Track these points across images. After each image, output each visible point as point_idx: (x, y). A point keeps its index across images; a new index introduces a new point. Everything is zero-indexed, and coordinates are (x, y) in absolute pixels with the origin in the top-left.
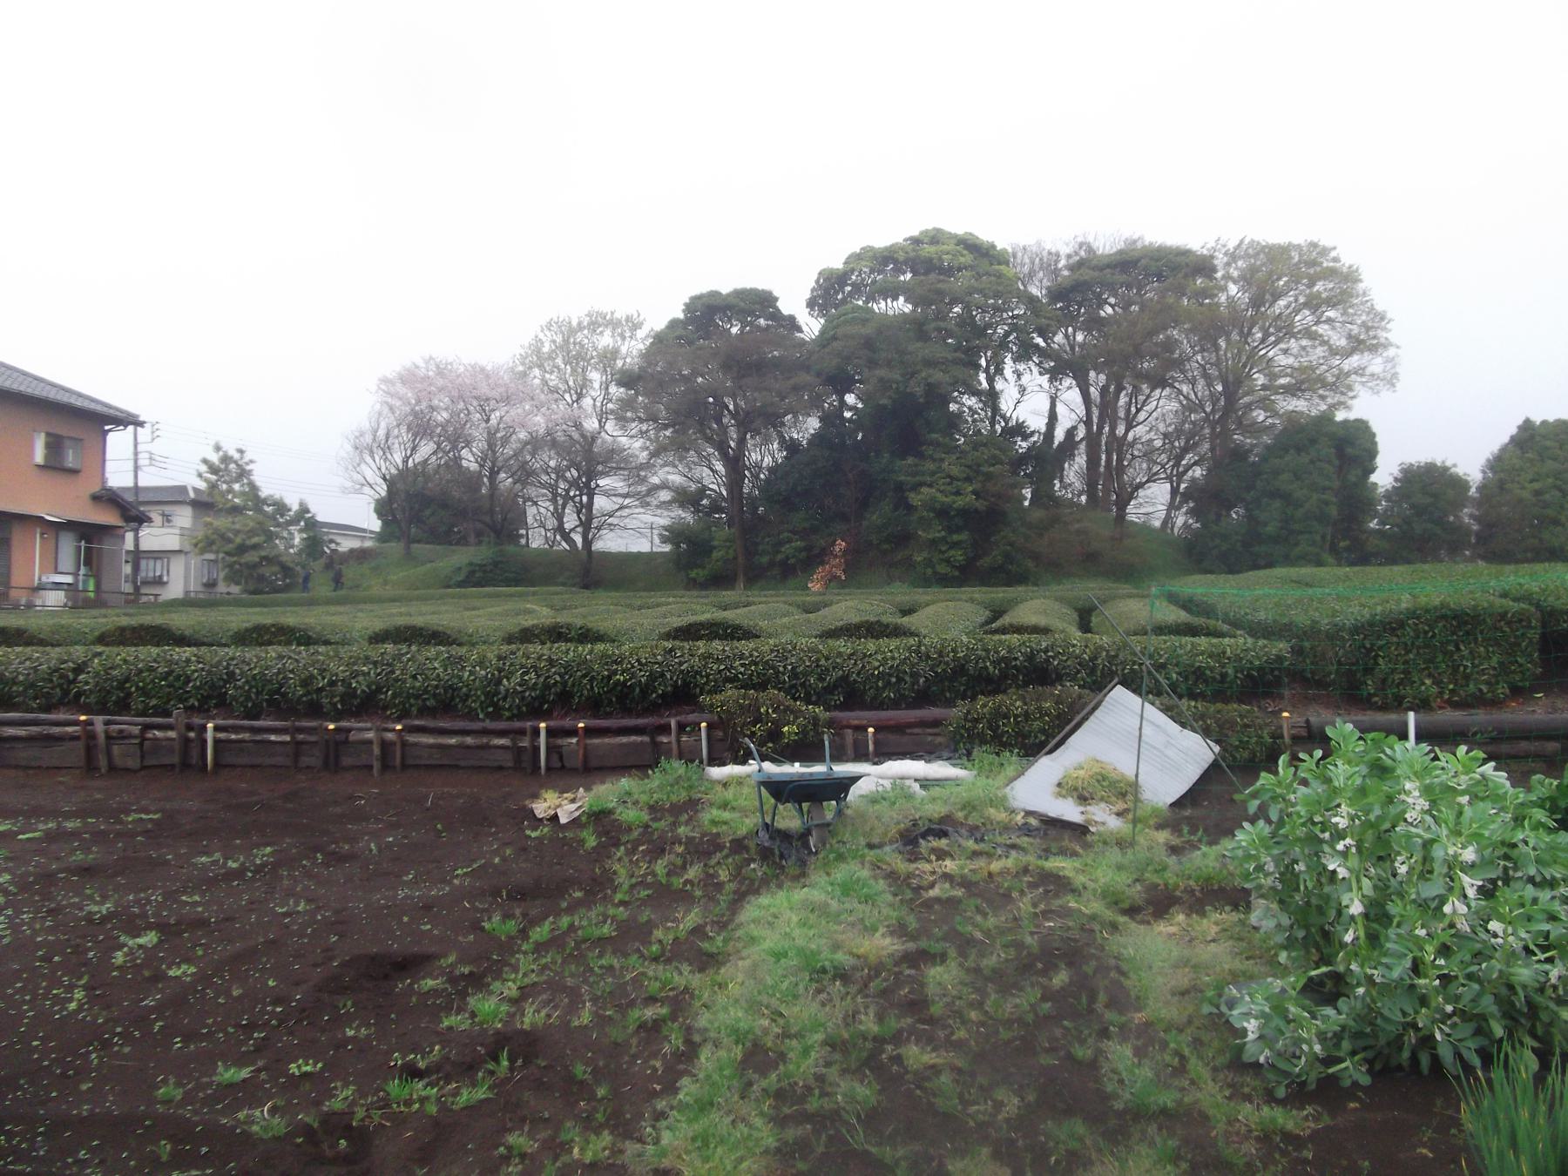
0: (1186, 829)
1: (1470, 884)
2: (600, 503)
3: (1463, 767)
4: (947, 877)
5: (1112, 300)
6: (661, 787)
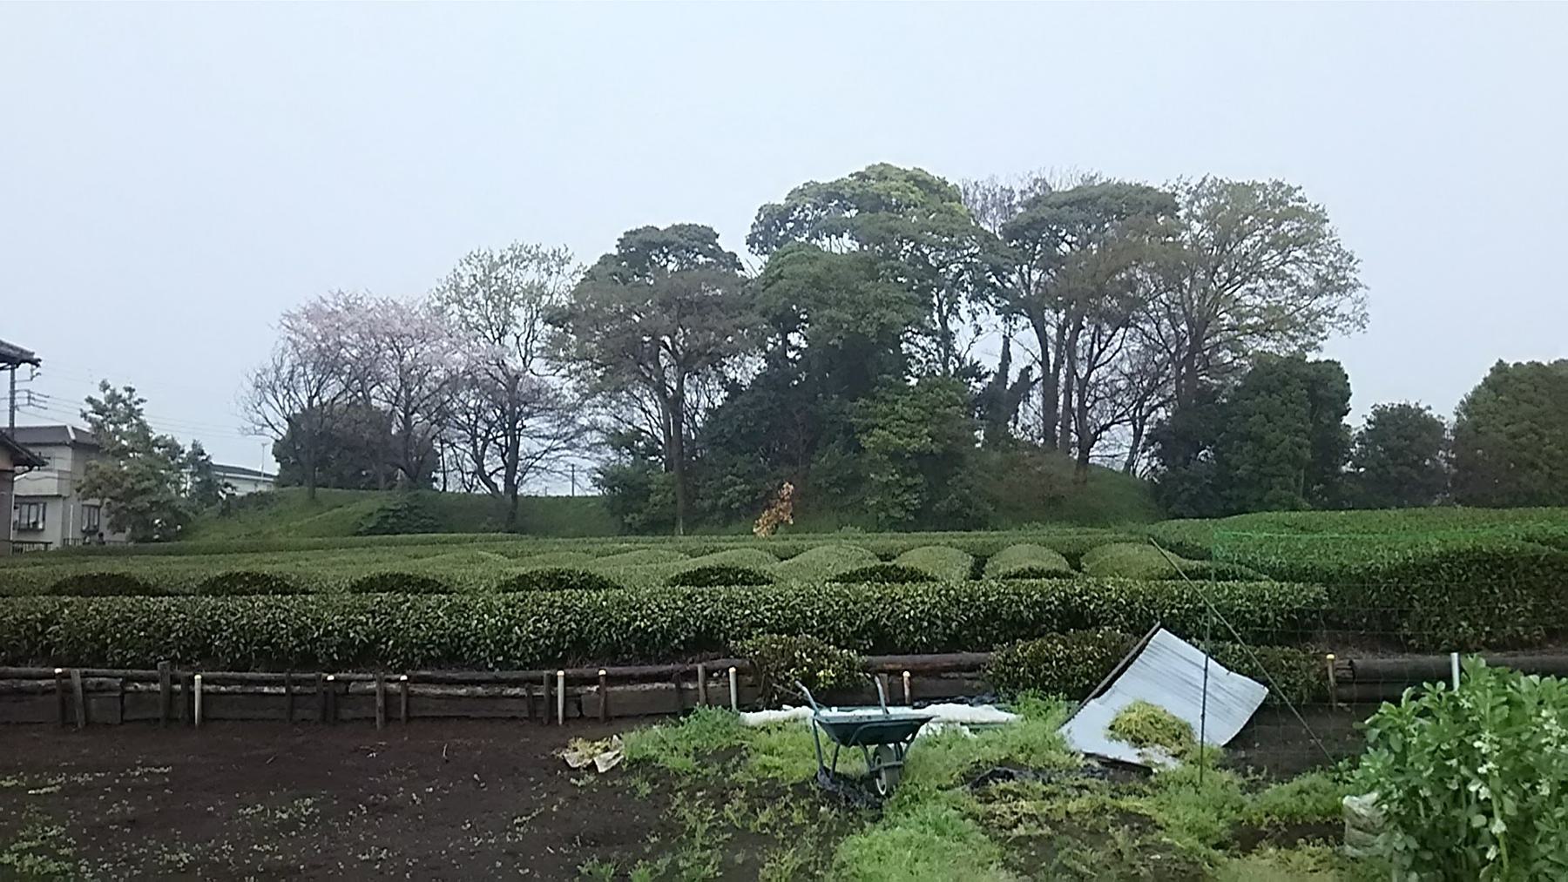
0: (1250, 769)
2: (525, 444)
5: (1069, 238)
6: (699, 733)
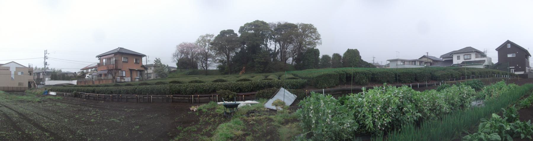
1: (330, 116)
2: (208, 62)
3: (330, 98)
4: (253, 120)
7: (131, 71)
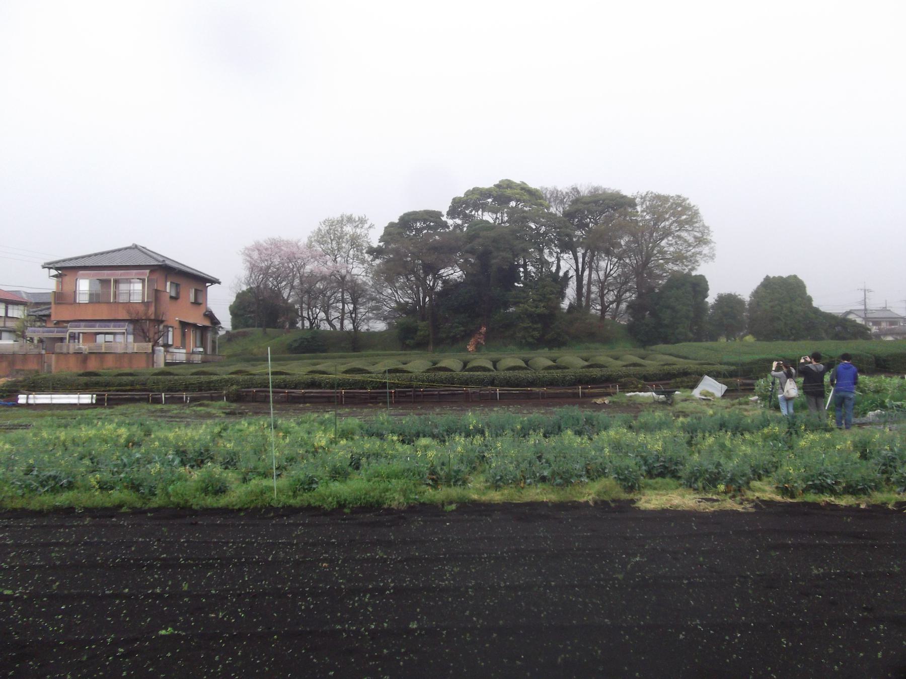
7: (184, 325)
